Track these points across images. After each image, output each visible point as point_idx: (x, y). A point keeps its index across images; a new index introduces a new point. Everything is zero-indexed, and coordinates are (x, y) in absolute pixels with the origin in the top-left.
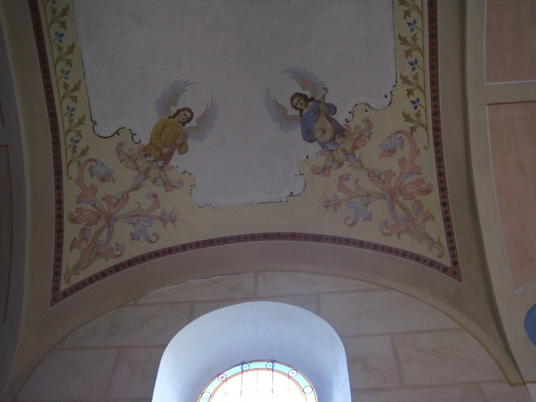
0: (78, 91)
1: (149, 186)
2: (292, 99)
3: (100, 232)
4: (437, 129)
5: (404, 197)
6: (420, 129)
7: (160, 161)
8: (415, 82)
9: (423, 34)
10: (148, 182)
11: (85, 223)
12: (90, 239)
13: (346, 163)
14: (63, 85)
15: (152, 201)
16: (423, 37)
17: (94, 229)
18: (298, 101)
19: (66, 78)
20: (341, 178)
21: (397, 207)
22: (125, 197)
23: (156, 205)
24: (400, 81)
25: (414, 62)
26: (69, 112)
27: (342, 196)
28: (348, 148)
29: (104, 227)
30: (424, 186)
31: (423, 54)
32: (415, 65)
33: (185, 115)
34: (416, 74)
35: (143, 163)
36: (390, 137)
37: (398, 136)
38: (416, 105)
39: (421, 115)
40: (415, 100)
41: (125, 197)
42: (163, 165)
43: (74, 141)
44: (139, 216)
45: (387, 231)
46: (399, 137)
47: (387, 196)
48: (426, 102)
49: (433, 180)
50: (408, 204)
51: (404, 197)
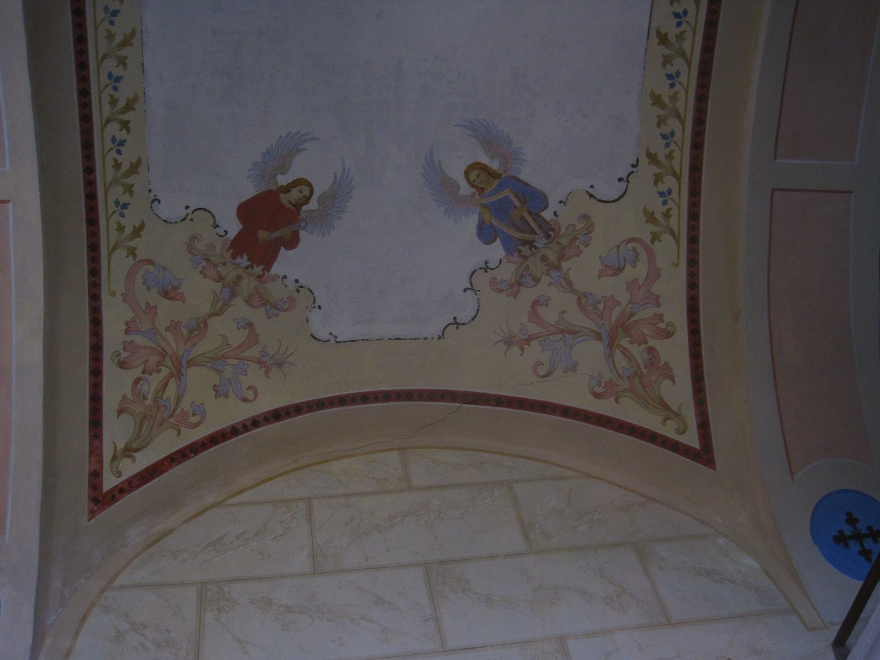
0: (138, 239)
1: (240, 309)
2: (467, 173)
3: (165, 384)
4: (693, 240)
5: (630, 339)
6: (667, 239)
7: (257, 266)
8: (663, 170)
9: (694, 32)
10: (238, 301)
11: (141, 368)
12: (150, 397)
13: (545, 279)
14: (115, 226)
15: (245, 333)
16: (687, 97)
17: (155, 380)
18: (478, 176)
19: (122, 215)
20: (536, 303)
21: (618, 355)
22: (202, 325)
23: (253, 339)
24: (644, 160)
25: (674, 74)
26: (115, 147)
27: (533, 329)
28: (552, 256)
29: (172, 375)
30: (662, 325)
31: (683, 123)
32: (676, 80)
33: (301, 192)
34: (682, 33)
35: (230, 272)
36: (618, 247)
37: (630, 246)
38: (668, 141)
39: (678, 99)
40: (674, 74)
41: (200, 327)
42: (261, 273)
43: (113, 79)
44: (225, 359)
45: (599, 390)
46: (631, 248)
47: (604, 337)
48: (690, 78)
49: (678, 315)
50: (637, 351)
51: (630, 339)
